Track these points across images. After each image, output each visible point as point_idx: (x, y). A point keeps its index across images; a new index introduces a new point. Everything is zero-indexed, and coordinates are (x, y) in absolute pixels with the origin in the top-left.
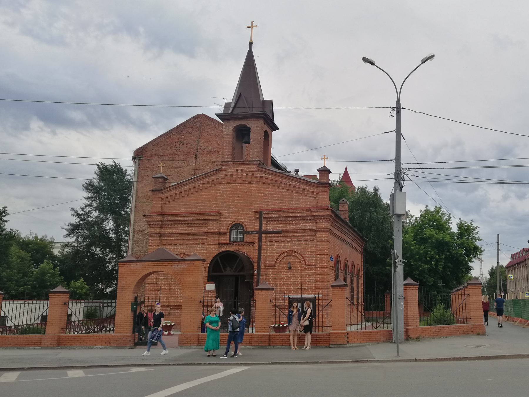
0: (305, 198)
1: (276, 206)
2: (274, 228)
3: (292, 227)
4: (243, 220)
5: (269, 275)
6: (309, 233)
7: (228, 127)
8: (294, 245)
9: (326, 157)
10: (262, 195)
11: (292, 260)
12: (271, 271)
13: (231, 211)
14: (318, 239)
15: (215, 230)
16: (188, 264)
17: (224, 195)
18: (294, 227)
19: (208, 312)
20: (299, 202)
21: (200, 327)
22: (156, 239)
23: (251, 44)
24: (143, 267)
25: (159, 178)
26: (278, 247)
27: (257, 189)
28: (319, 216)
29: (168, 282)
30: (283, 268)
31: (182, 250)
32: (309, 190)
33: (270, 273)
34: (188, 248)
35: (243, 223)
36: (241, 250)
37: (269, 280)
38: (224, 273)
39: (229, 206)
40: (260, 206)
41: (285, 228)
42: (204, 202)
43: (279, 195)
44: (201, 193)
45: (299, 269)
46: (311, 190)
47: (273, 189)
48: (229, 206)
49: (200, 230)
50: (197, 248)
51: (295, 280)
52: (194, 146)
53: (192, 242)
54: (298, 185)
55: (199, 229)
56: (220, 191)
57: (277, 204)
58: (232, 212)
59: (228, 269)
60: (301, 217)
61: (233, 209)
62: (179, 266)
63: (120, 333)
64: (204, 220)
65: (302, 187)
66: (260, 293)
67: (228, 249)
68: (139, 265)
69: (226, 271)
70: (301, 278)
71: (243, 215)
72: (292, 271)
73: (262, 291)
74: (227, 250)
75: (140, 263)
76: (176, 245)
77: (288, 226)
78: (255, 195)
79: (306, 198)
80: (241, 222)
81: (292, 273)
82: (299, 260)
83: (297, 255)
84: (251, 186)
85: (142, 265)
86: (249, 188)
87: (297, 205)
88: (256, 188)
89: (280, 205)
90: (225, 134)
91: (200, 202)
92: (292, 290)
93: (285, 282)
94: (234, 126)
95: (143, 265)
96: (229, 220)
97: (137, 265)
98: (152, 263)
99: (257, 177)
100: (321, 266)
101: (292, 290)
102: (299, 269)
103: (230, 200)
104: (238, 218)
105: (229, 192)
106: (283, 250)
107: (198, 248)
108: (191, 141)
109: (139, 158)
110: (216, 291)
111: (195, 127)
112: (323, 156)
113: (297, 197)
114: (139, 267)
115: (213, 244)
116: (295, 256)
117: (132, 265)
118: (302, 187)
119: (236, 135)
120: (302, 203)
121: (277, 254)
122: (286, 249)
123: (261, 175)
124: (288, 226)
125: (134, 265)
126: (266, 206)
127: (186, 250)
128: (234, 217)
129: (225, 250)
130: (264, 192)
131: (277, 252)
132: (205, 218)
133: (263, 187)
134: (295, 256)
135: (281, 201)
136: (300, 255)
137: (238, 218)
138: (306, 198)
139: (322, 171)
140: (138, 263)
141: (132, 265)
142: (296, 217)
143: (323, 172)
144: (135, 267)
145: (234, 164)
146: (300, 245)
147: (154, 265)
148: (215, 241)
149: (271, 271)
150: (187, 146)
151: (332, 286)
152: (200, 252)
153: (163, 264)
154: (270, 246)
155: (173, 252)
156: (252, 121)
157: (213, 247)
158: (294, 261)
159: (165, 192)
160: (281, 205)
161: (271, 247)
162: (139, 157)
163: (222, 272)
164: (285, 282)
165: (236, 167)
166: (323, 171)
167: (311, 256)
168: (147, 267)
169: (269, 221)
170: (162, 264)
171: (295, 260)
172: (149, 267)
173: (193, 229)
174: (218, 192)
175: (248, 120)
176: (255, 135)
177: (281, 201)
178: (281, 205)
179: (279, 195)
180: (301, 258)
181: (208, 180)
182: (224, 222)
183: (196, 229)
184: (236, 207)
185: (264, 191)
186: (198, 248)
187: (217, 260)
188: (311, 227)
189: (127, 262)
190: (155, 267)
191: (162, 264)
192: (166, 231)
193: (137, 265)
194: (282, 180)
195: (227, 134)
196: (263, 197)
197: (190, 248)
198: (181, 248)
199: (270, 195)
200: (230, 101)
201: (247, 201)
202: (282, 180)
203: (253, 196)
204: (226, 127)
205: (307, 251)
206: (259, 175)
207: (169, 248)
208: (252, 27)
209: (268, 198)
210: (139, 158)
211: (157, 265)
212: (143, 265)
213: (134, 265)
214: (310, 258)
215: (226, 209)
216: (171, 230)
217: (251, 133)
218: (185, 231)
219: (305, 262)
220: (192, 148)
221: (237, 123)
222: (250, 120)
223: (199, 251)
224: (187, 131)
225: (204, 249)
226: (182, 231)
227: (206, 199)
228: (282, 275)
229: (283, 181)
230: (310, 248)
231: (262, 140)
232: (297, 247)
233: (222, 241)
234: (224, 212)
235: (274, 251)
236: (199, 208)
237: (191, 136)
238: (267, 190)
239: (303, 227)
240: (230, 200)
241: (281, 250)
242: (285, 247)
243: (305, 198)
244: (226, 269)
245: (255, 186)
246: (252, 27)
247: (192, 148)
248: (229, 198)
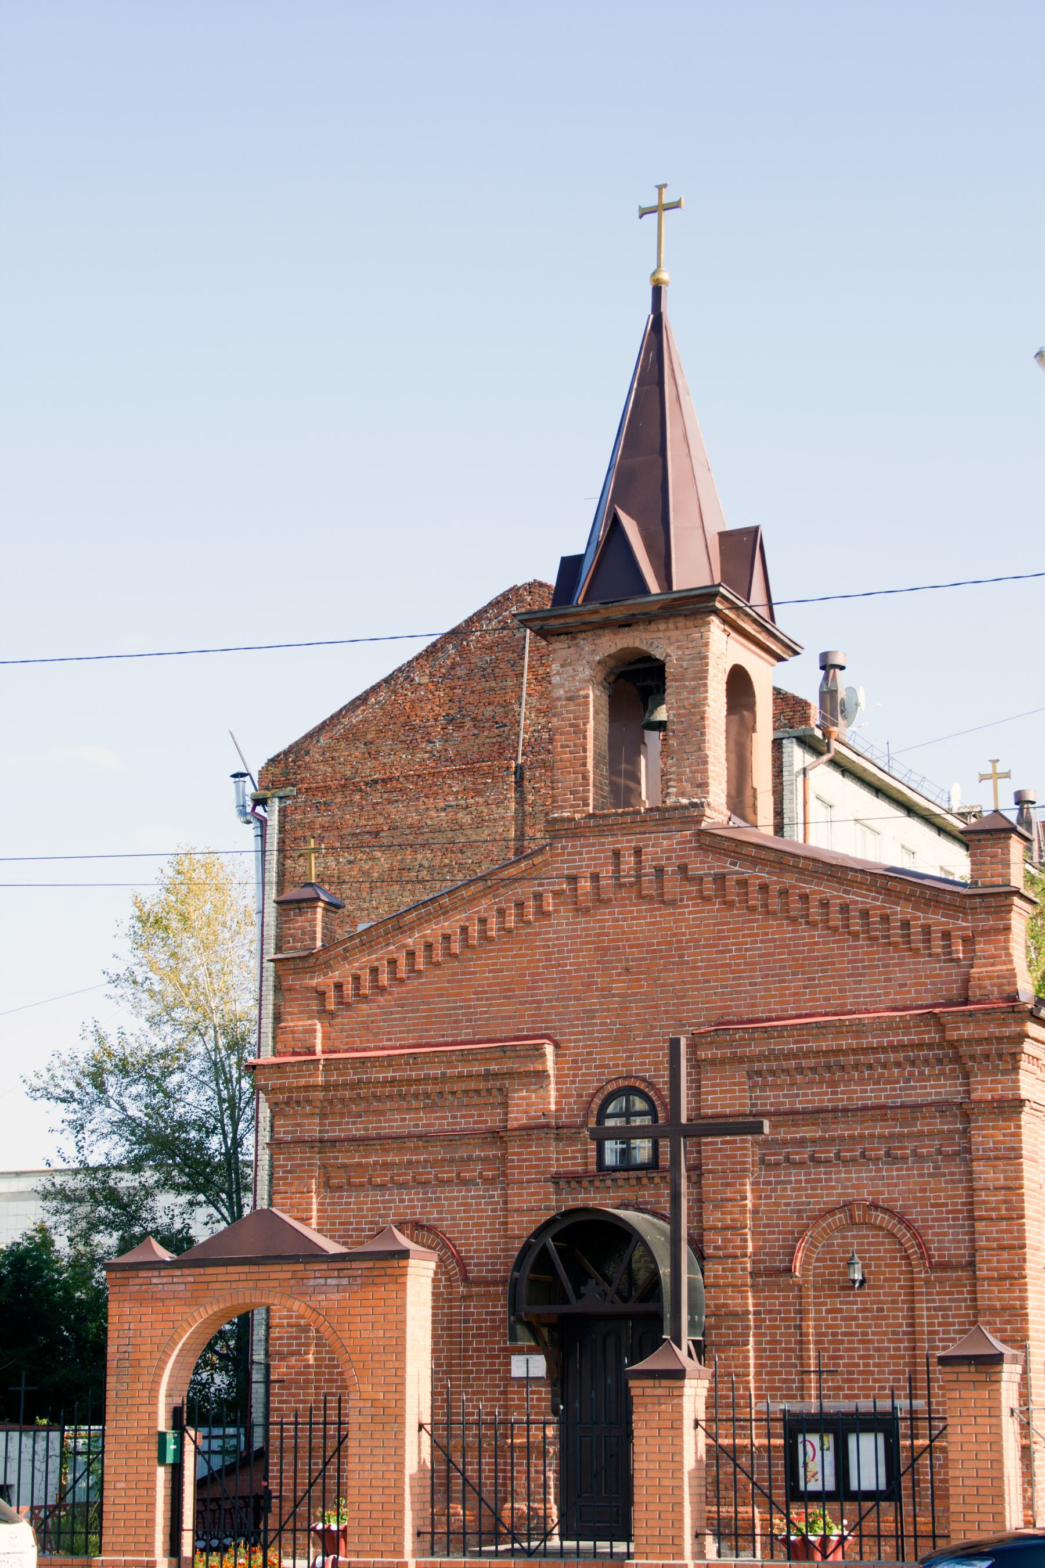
0: (915, 963)
1: (788, 1002)
2: (784, 1103)
3: (858, 1099)
4: (649, 1070)
5: (770, 1312)
6: (935, 1124)
7: (570, 664)
8: (872, 1179)
9: (1001, 768)
10: (725, 958)
11: (870, 1244)
12: (777, 1297)
13: (599, 1031)
14: (978, 1150)
15: (535, 1118)
16: (365, 1273)
17: (565, 965)
18: (870, 1098)
19: (461, 1467)
20: (887, 980)
21: (422, 1530)
22: (303, 1165)
23: (657, 292)
24: (195, 1287)
25: (304, 905)
26: (806, 1189)
27: (700, 933)
28: (979, 1041)
29: (450, 1351)
30: (829, 1281)
31: (408, 1207)
32: (929, 926)
33: (774, 1304)
34: (430, 1199)
35: (650, 1083)
36: (647, 1203)
37: (773, 1335)
38: (575, 1306)
39: (591, 1014)
40: (721, 1008)
41: (829, 1101)
42: (487, 999)
43: (798, 952)
44: (471, 960)
45: (900, 1287)
46: (936, 925)
47: (771, 926)
48: (591, 1014)
49: (475, 1122)
50: (464, 1197)
51: (885, 1333)
52: (506, 729)
53: (810, 1132)
54: (879, 903)
55: (472, 1116)
56: (548, 947)
57: (791, 995)
58: (604, 1038)
59: (590, 1288)
60: (898, 1052)
61: (605, 1024)
62: (329, 1281)
63: (125, 1553)
64: (488, 1075)
65: (896, 913)
66: (648, 1392)
67: (595, 1199)
68: (180, 1280)
69: (584, 1295)
70: (912, 1325)
71: (652, 1049)
72: (868, 1295)
73: (657, 1382)
74: (591, 1204)
75: (186, 1271)
76: (383, 1186)
77: (843, 1092)
78: (695, 961)
79: (918, 963)
80: (643, 1079)
81: (873, 1302)
82: (901, 1244)
83: (890, 1223)
84: (676, 921)
85: (191, 1279)
86: (670, 928)
87: (879, 995)
88: (698, 926)
89: (806, 1001)
90: (558, 699)
91: (470, 1000)
92: (875, 1381)
93: (842, 1342)
94: (597, 658)
95: (199, 1279)
96: (595, 1074)
97: (175, 1280)
98: (231, 1269)
99: (700, 880)
100: (996, 1269)
101: (875, 1381)
102: (900, 1287)
103: (590, 984)
104: (631, 1065)
105: (587, 950)
106: (825, 1203)
107: (472, 1197)
108: (490, 708)
109: (281, 798)
110: (553, 1385)
111: (507, 643)
112: (990, 764)
113: (879, 960)
114: (182, 1287)
115: (529, 1181)
116: (881, 1228)
117: (154, 1281)
118: (896, 913)
119: (610, 696)
120: (901, 986)
121: (799, 1218)
122: (839, 1195)
123: (719, 867)
124: (843, 1092)
125: (165, 1280)
126: (746, 1006)
127: (425, 1206)
128: (610, 1059)
129: (579, 1204)
130: (733, 944)
131: (800, 1211)
132: (494, 1067)
133: (728, 923)
134: (881, 1228)
135: (810, 979)
136: (901, 1221)
137: (631, 1065)
138: (918, 963)
139: (981, 837)
140: (178, 1272)
141: (154, 1281)
142: (875, 1050)
143: (985, 840)
144: (166, 1287)
145: (601, 828)
146: (899, 1177)
147: (236, 1277)
148: (537, 1166)
149: (777, 1297)
150: (476, 732)
151: (943, 1361)
152: (479, 1218)
153: (273, 1276)
154: (769, 1183)
155: (373, 1216)
156: (668, 634)
157: (533, 1194)
158: (879, 1251)
159: (327, 965)
160: (810, 1000)
161: (774, 1190)
162: (281, 794)
163: (566, 1301)
164: (842, 1342)
165: (609, 842)
166: (988, 836)
167: (949, 1227)
168: (212, 1286)
169: (759, 1073)
170: (266, 1276)
171: (883, 1244)
172: (217, 1286)
173: (445, 1118)
174: (541, 954)
175: (653, 627)
176: (685, 694)
177: (810, 979)
178: (810, 1000)
179: (798, 952)
180: (905, 1235)
181: (500, 902)
182: (573, 1082)
183: (462, 1117)
184: (618, 1016)
185: (734, 937)
186: (472, 1197)
187: (545, 1249)
188: (946, 1092)
189: (160, 1269)
190: (240, 1285)
191: (266, 1276)
192: (340, 1131)
193: (175, 1280)
194: (808, 888)
195: (569, 695)
196: (729, 965)
197: (438, 1199)
198: (402, 1201)
199: (760, 956)
200: (578, 548)
201: (664, 985)
202: (808, 888)
203: (687, 962)
204: (562, 666)
205: (933, 1205)
206: (709, 868)
207: (355, 1203)
208: (660, 209)
209: (751, 970)
210: (281, 798)
211: (250, 1276)
212: (199, 1279)
213: (165, 1280)
214: (946, 1234)
215: (577, 1026)
216: (361, 1123)
217: (668, 684)
218: (417, 1126)
219: (925, 1254)
220: (499, 740)
221: (611, 644)
222: (662, 626)
223: (477, 1211)
224: (473, 666)
225: (498, 1203)
226: (404, 1127)
227: (495, 984)
228: (828, 1311)
229: (814, 892)
230: (945, 1190)
231: (720, 712)
232: (889, 1185)
233: (567, 1165)
234: (570, 1041)
235: (787, 1204)
236: (467, 1027)
237: (493, 684)
238: (744, 936)
239: (910, 1095)
240: (590, 984)
241: (815, 1203)
242: (833, 1188)
243: (915, 963)
244: (583, 1289)
245: (694, 919)
246: (660, 209)
247: (499, 740)
248: (590, 976)
